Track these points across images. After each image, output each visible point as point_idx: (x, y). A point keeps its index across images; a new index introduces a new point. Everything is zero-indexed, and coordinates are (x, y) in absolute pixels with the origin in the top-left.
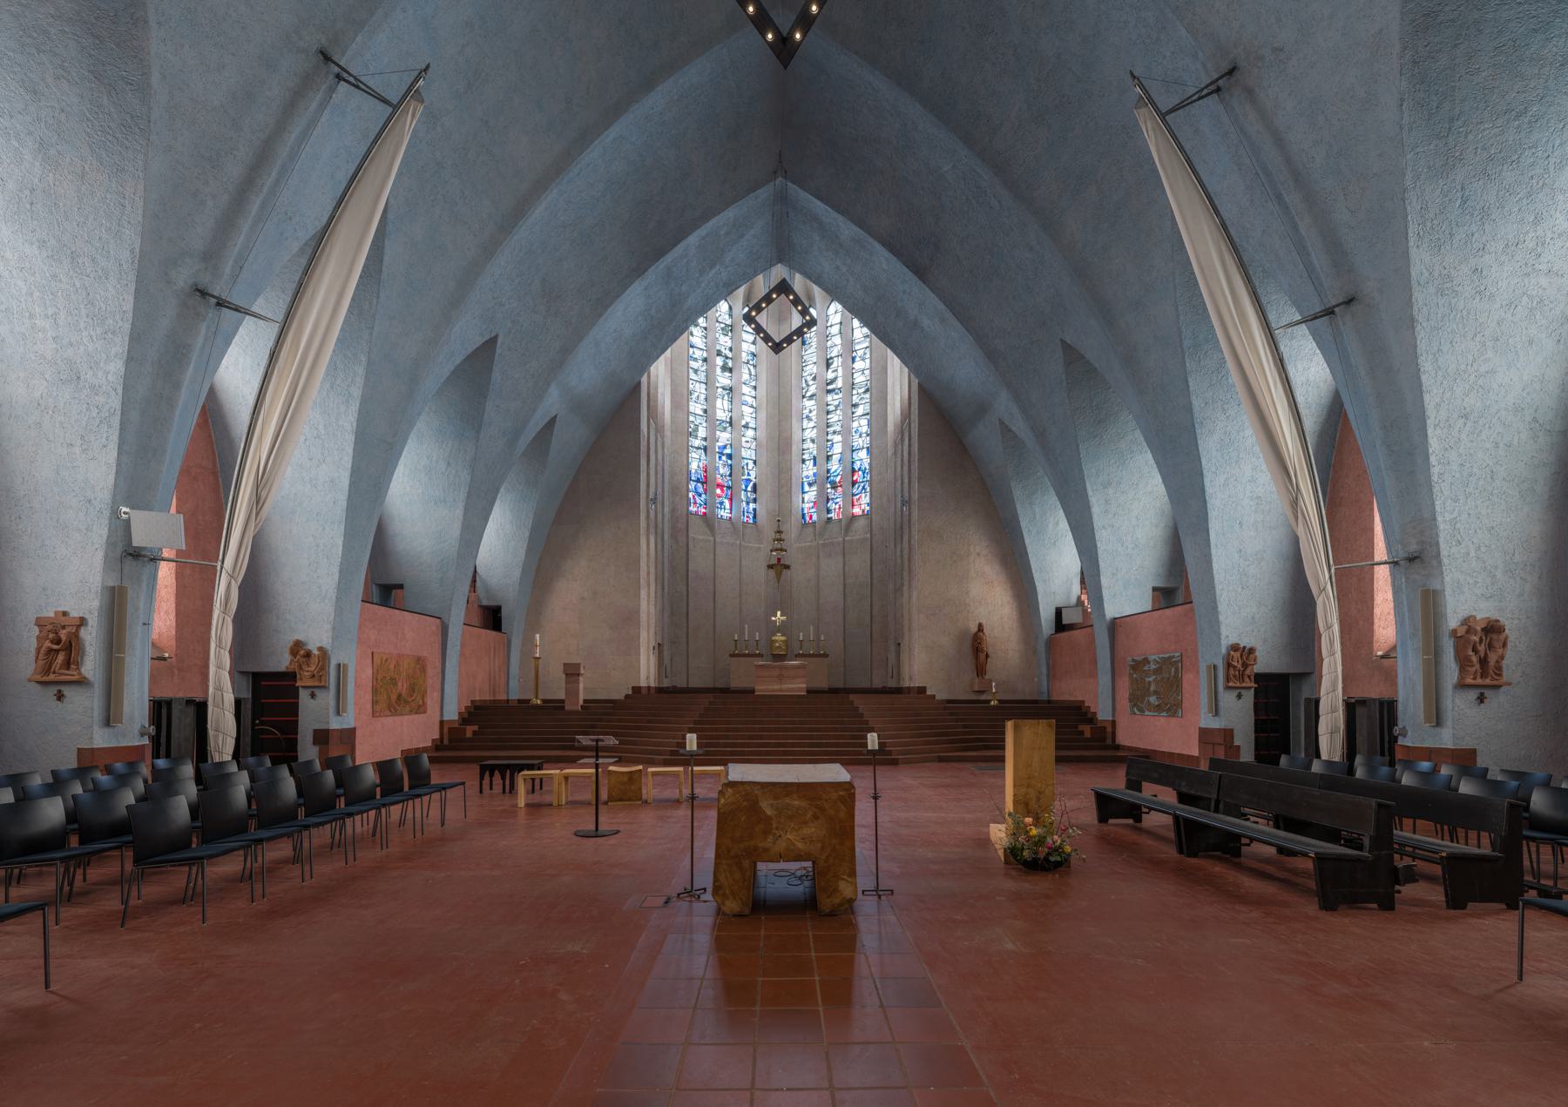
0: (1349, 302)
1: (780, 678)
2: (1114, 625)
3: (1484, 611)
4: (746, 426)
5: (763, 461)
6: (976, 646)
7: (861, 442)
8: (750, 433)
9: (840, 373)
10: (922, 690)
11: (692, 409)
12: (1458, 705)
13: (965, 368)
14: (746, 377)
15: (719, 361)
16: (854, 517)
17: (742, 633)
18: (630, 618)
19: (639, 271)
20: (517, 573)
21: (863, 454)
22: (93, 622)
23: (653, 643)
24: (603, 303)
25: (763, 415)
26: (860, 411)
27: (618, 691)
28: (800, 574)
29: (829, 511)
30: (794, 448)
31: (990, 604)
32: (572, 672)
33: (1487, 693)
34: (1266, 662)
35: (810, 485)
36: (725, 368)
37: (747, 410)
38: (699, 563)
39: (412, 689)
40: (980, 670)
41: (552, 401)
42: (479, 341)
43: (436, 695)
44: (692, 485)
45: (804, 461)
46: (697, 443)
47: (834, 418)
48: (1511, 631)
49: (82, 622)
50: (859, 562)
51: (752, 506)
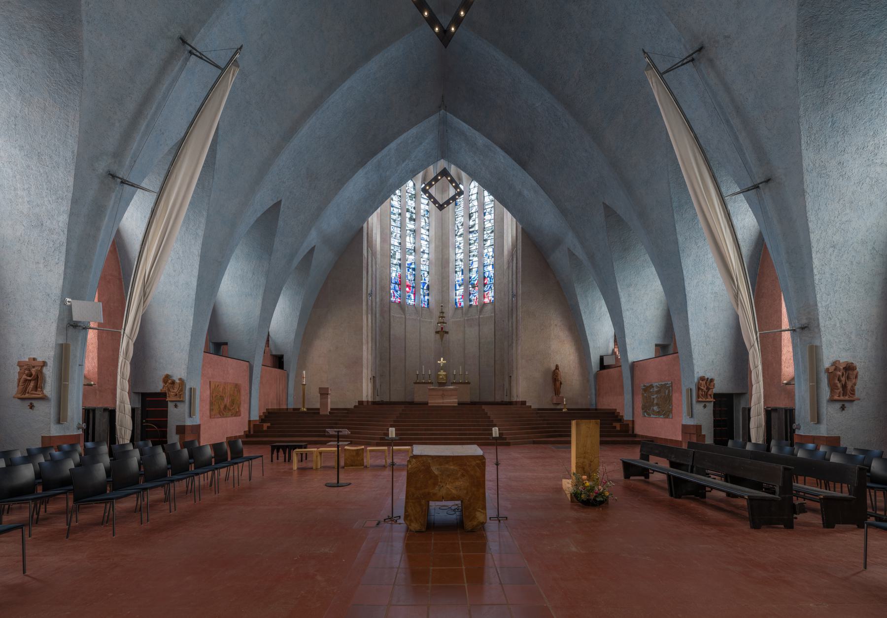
0: (768, 181)
1: (443, 396)
2: (633, 366)
3: (844, 358)
4: (423, 252)
5: (433, 272)
6: (555, 378)
7: (489, 261)
8: (426, 256)
9: (477, 222)
10: (524, 403)
11: (392, 242)
12: (830, 411)
13: (548, 219)
14: (423, 224)
15: (408, 215)
16: (485, 304)
17: (421, 370)
18: (357, 362)
19: (362, 163)
20: (292, 336)
21: (490, 268)
22: (51, 363)
23: (370, 376)
24: (341, 182)
25: (433, 245)
26: (488, 243)
27: (351, 405)
28: (454, 337)
29: (470, 301)
30: (451, 265)
31: (563, 354)
32: (324, 393)
33: (846, 404)
34: (720, 386)
35: (460, 286)
36: (411, 219)
37: (424, 243)
38: (397, 330)
39: (233, 402)
40: (557, 391)
41: (313, 239)
42: (271, 203)
43: (246, 406)
44: (392, 286)
45: (456, 272)
46: (395, 262)
47: (473, 247)
48: (859, 366)
49: (44, 364)
50: (488, 330)
51: (426, 298)
